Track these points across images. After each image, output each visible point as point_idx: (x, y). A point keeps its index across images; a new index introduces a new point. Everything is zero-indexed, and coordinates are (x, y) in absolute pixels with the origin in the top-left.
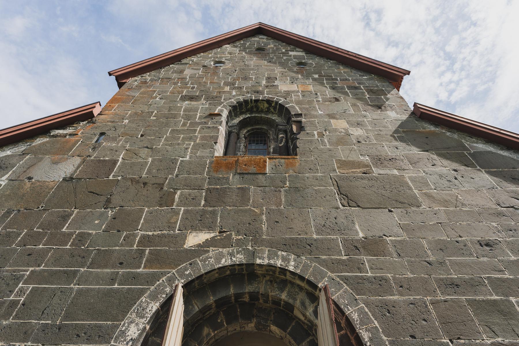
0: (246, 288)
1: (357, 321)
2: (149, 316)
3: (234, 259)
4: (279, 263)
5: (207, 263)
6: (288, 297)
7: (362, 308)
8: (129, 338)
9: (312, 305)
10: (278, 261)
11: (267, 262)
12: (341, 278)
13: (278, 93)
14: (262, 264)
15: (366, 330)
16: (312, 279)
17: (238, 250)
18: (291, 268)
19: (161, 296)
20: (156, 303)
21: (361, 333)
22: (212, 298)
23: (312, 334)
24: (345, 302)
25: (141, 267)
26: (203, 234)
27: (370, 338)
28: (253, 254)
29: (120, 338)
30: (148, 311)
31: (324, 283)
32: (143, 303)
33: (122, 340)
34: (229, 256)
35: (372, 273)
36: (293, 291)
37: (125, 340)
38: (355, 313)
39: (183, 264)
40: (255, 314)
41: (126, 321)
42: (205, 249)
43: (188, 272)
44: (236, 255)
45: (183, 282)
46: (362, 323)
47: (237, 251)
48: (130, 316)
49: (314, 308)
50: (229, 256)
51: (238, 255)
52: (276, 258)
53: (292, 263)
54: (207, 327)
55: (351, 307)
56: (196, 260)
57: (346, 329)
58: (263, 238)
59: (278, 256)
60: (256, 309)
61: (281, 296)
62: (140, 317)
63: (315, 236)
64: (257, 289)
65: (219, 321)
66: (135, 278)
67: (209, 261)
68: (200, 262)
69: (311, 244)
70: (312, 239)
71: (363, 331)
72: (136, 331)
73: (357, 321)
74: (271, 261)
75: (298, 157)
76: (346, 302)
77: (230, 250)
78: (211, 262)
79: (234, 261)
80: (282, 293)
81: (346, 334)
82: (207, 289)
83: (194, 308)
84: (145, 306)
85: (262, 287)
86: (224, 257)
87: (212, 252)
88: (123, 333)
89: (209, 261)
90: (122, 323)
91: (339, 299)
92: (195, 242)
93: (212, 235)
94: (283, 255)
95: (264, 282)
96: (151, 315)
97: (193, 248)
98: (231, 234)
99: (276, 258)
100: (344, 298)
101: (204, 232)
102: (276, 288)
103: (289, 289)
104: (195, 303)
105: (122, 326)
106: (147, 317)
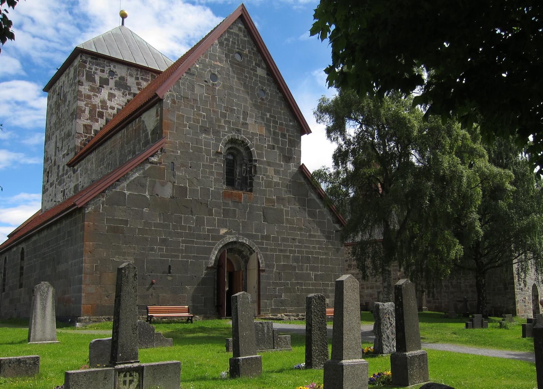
4: (244, 241)
13: (152, 359)
16: (252, 247)
18: (247, 243)
25: (104, 116)
28: (238, 238)
63: (254, 233)
66: (209, 244)
70: (253, 234)
75: (253, 193)
87: (228, 236)
88: (211, 258)
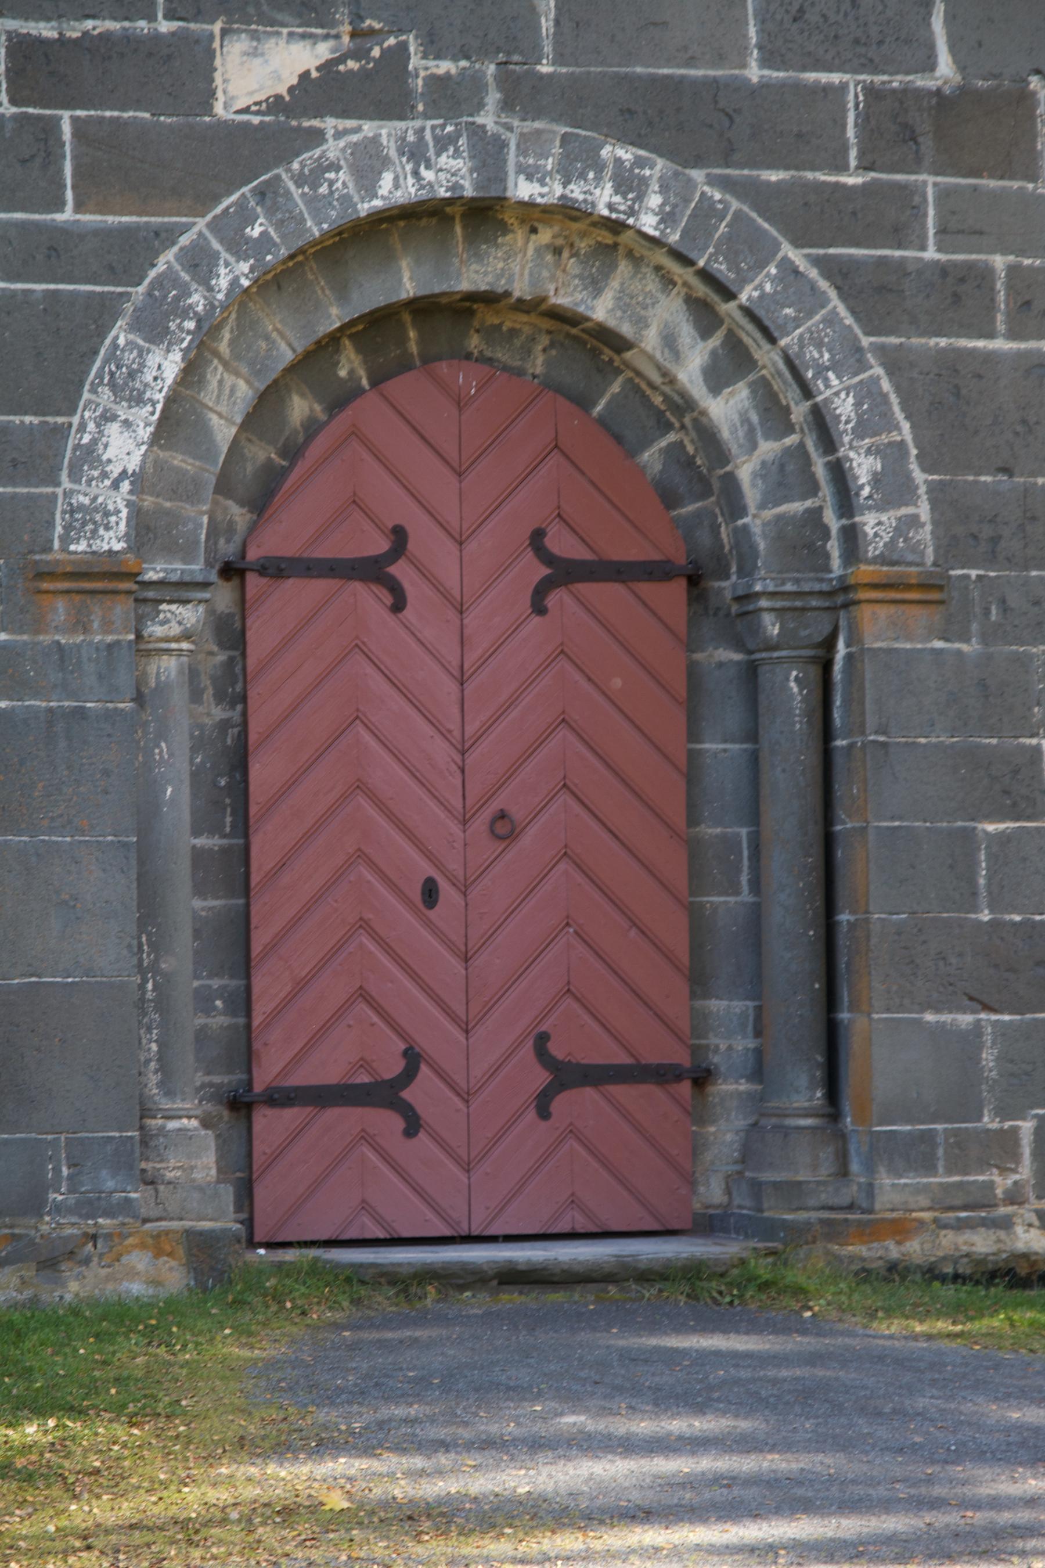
0: (459, 274)
1: (847, 422)
2: (160, 397)
3: (428, 175)
5: (323, 190)
6: (619, 314)
7: (876, 380)
8: (115, 470)
9: (701, 345)
10: (598, 192)
11: (558, 190)
12: (827, 267)
14: (539, 200)
15: (869, 452)
17: (438, 131)
18: (648, 223)
19: (180, 327)
20: (168, 351)
21: (851, 460)
22: (334, 311)
23: (677, 425)
24: (822, 356)
26: (282, 43)
27: (875, 474)
29: (86, 468)
30: (149, 378)
31: (760, 287)
32: (123, 351)
33: (96, 473)
34: (408, 161)
35: (939, 250)
36: (636, 292)
37: (105, 475)
38: (848, 395)
39: (230, 193)
40: (476, 351)
41: (87, 414)
42: (306, 124)
43: (807, 632)
44: (433, 158)
45: (246, 270)
46: (862, 429)
47: (435, 138)
48: (93, 397)
49: (706, 357)
50: (408, 161)
51: (443, 158)
52: (591, 175)
53: (655, 200)
54: (303, 395)
55: (839, 377)
56: (278, 177)
57: (802, 430)
58: (542, 77)
59: (599, 167)
60: (478, 331)
61: (592, 308)
62: (129, 400)
63: (754, 72)
64: (503, 282)
65: (343, 373)
67: (331, 183)
68: (299, 185)
69: (735, 110)
70: (741, 86)
71: (859, 454)
72: (132, 447)
73: (847, 422)
74: (572, 186)
76: (827, 356)
77: (408, 128)
78: (339, 184)
79: (430, 183)
80: (595, 298)
81: (802, 445)
82: (310, 277)
83: (278, 349)
84: (133, 362)
85: (522, 275)
86: (385, 162)
89: (331, 183)
90: (76, 420)
91: (802, 346)
92: (256, 86)
93: (324, 51)
94: (618, 161)
95: (530, 252)
96: (163, 394)
97: (256, 120)
98: (403, 47)
99: (591, 175)
100: (819, 345)
101: (285, 31)
102: (575, 276)
103: (622, 284)
104: (276, 330)
105: (78, 431)
106: (154, 404)
